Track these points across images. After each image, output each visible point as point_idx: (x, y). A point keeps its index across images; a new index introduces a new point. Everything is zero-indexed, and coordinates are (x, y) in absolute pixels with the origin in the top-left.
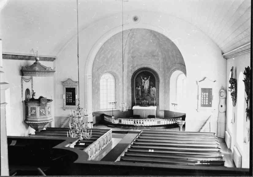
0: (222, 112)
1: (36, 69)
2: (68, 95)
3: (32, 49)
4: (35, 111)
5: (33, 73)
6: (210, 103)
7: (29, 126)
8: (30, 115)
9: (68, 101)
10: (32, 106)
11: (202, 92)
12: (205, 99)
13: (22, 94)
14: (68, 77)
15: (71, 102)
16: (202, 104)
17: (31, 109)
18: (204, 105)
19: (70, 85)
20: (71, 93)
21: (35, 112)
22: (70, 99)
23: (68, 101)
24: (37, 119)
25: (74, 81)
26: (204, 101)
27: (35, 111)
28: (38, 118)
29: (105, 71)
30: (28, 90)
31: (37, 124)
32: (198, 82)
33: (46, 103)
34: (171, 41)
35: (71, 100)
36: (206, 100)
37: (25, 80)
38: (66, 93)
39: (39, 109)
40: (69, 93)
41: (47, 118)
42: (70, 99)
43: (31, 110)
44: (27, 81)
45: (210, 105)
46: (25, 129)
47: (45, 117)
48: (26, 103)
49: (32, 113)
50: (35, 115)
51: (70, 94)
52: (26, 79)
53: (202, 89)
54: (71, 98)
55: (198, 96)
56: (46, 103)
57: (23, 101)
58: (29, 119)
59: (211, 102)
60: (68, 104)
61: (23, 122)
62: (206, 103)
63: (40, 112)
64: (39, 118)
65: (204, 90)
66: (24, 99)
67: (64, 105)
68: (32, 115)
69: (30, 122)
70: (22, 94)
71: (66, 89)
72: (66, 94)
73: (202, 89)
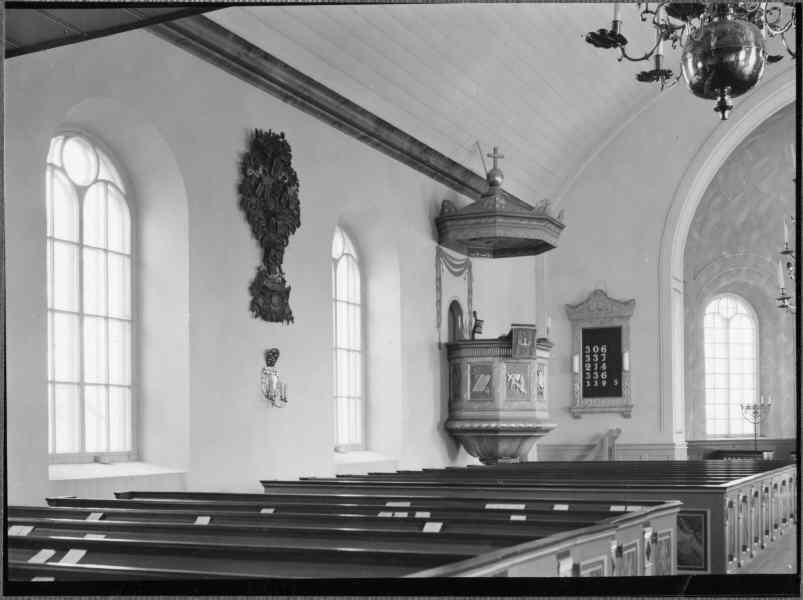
1: (497, 206)
3: (477, 143)
4: (488, 378)
5: (483, 220)
6: (616, 382)
7: (458, 448)
8: (467, 395)
9: (592, 381)
10: (474, 360)
12: (596, 368)
13: (439, 313)
14: (592, 288)
15: (604, 383)
17: (472, 371)
19: (603, 314)
20: (604, 349)
21: (489, 385)
22: (600, 371)
23: (592, 381)
24: (498, 410)
25: (617, 298)
27: (488, 378)
29: (724, 283)
30: (455, 308)
31: (496, 430)
33: (533, 345)
35: (604, 375)
37: (451, 267)
38: (584, 350)
39: (504, 372)
40: (596, 349)
41: (534, 410)
42: (600, 374)
43: (472, 377)
44: (454, 270)
47: (524, 404)
48: (452, 352)
49: (475, 389)
50: (488, 395)
51: (600, 353)
52: (452, 264)
54: (604, 367)
56: (533, 345)
57: (440, 344)
58: (465, 414)
60: (589, 392)
61: (438, 428)
63: (509, 383)
64: (503, 410)
66: (445, 339)
67: (574, 399)
68: (474, 395)
69: (467, 425)
70: (439, 313)
71: (586, 332)
72: (584, 354)
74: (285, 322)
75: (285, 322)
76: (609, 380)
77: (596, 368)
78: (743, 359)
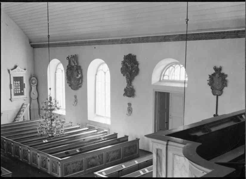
0: (34, 99)
2: (16, 85)
6: (22, 91)
11: (14, 81)
12: (17, 88)
16: (15, 93)
18: (16, 94)
20: (19, 82)
22: (18, 88)
26: (16, 90)
28: (184, 86)
32: (10, 71)
34: (231, 38)
36: (18, 88)
40: (17, 82)
42: (18, 89)
45: (22, 94)
46: (227, 87)
51: (18, 83)
53: (14, 78)
54: (19, 87)
55: (11, 85)
59: (23, 90)
62: (18, 92)
65: (16, 79)
73: (14, 78)
74: (227, 78)
75: (227, 78)
76: (21, 91)
77: (17, 87)
78: (49, 42)
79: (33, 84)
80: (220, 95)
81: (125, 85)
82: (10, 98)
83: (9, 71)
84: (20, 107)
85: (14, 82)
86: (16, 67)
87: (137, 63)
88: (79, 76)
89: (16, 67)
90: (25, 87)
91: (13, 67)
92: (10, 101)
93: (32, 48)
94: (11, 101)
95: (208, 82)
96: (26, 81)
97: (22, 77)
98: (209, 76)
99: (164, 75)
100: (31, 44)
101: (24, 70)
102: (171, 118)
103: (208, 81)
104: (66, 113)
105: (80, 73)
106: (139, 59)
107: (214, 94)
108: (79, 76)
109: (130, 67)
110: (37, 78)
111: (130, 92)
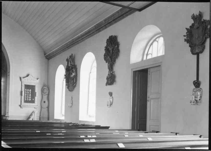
6: (33, 99)
11: (25, 88)
18: (26, 101)
32: (22, 78)
45: (33, 102)
51: (29, 91)
54: (30, 95)
55: (21, 92)
62: (29, 100)
65: (27, 87)
73: (26, 85)
76: (32, 99)
79: (44, 93)
80: (201, 52)
81: (106, 72)
82: (20, 104)
83: (21, 78)
84: (30, 114)
85: (25, 90)
86: (28, 76)
87: (118, 44)
88: (73, 74)
89: (28, 76)
90: (36, 96)
91: (25, 75)
92: (20, 107)
93: (47, 60)
94: (21, 107)
95: (185, 38)
96: (38, 90)
97: (34, 86)
98: (186, 30)
99: (147, 55)
100: (46, 55)
101: (37, 80)
102: (149, 101)
103: (184, 36)
104: (65, 118)
105: (75, 72)
106: (119, 40)
107: (193, 54)
108: (73, 74)
109: (112, 51)
110: (49, 90)
111: (111, 80)
